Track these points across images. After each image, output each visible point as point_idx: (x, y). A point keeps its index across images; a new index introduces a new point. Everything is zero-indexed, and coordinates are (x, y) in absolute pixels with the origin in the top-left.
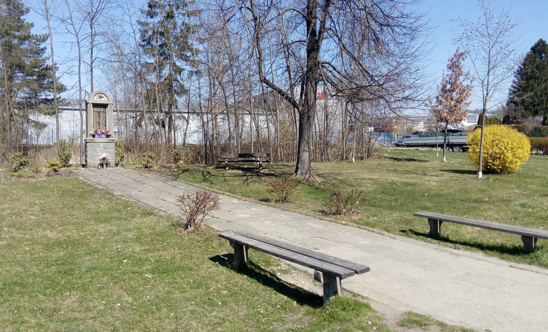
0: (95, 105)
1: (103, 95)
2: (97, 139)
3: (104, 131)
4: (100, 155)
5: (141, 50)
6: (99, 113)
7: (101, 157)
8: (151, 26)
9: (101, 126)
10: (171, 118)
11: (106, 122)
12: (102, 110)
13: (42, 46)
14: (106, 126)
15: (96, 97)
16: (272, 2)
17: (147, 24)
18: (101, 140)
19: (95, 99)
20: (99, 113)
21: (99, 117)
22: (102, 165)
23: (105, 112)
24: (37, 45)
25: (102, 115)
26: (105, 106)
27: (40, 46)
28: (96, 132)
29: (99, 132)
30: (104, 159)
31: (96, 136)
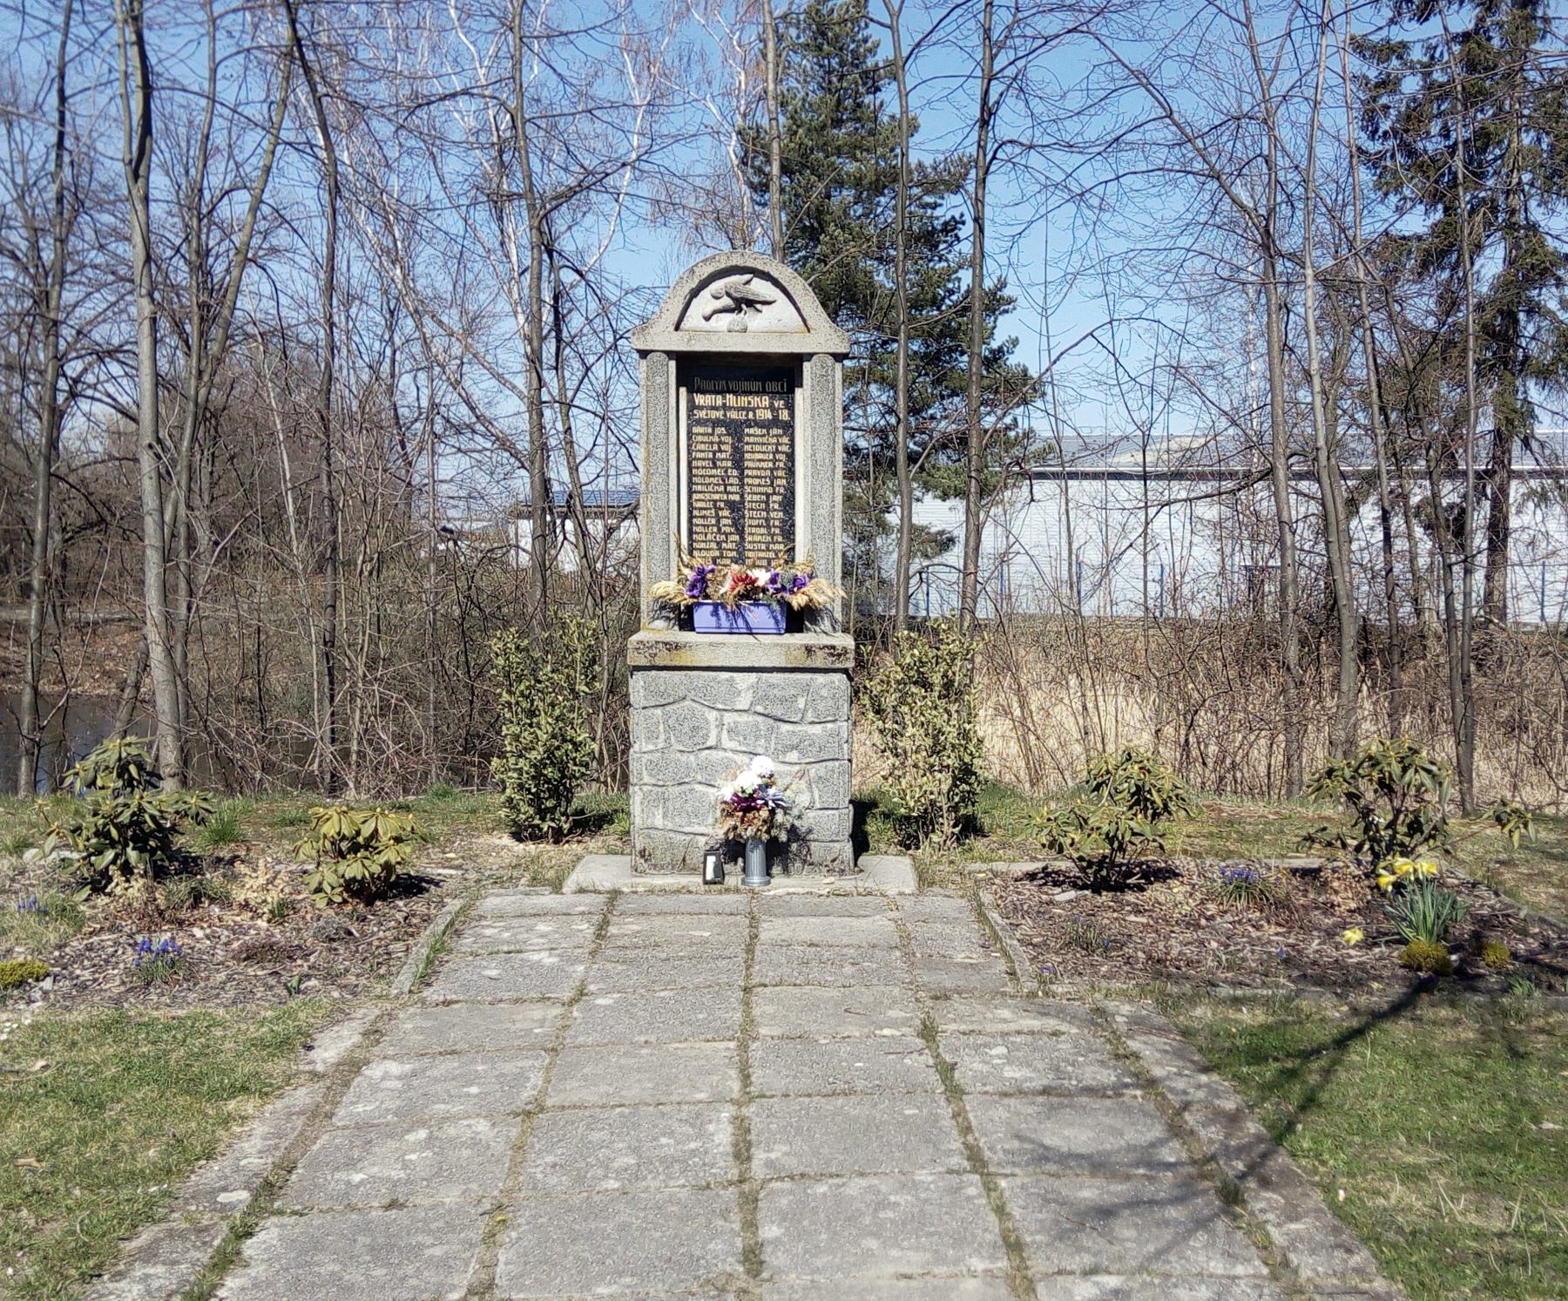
0: (698, 370)
1: (760, 288)
2: (703, 644)
3: (762, 577)
4: (732, 770)
5: (1365, 176)
6: (736, 430)
7: (727, 792)
8: (1417, 54)
9: (756, 535)
10: (1499, 504)
11: (788, 504)
12: (762, 407)
13: (943, 214)
14: (788, 532)
15: (704, 303)
16: (1562, 973)
17: (1400, 50)
18: (736, 649)
19: (694, 319)
20: (736, 430)
21: (738, 461)
22: (733, 850)
23: (789, 428)
24: (925, 206)
25: (760, 451)
26: (779, 373)
27: (938, 212)
28: (701, 583)
29: (725, 588)
30: (745, 804)
31: (702, 616)
